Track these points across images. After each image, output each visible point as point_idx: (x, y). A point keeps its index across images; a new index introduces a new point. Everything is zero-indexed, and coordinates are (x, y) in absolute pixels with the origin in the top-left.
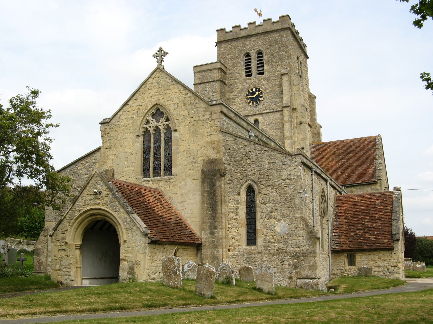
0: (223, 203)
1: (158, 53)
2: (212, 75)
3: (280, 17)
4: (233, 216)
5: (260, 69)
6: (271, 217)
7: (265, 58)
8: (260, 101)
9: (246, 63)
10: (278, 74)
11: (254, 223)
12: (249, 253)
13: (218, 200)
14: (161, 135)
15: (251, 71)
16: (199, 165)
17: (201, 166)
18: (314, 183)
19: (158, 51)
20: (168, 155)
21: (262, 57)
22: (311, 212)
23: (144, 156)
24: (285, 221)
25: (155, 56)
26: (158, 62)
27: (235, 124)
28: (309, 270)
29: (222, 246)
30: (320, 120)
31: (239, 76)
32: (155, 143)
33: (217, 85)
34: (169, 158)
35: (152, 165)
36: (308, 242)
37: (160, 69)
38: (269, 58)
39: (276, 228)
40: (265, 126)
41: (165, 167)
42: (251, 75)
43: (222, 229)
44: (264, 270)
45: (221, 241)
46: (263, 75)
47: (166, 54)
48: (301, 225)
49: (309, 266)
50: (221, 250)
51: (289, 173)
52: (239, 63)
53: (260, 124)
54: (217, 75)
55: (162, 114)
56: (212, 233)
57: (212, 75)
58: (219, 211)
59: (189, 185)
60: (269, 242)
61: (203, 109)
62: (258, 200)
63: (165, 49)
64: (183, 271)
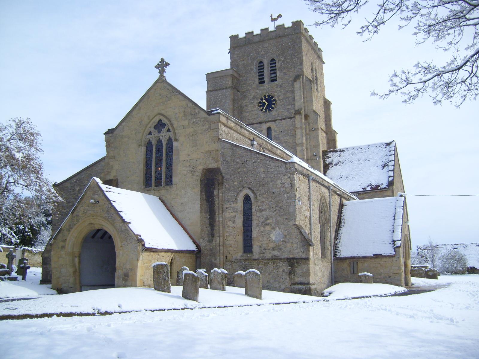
0: (221, 212)
1: (160, 64)
2: (224, 82)
3: (246, 34)
4: (230, 223)
5: (273, 75)
6: (267, 224)
7: (278, 65)
8: (272, 108)
9: (259, 70)
10: (291, 81)
11: (250, 231)
12: (245, 260)
13: (216, 209)
14: (162, 146)
15: (263, 78)
16: (198, 174)
17: (200, 175)
18: (311, 191)
19: (160, 62)
20: (169, 165)
21: (275, 63)
22: (307, 220)
23: (146, 166)
24: (279, 229)
25: (157, 67)
26: (159, 72)
27: (235, 133)
28: (303, 276)
29: (220, 253)
30: (335, 126)
31: (252, 83)
32: (156, 154)
33: (229, 92)
34: (170, 167)
35: (153, 175)
36: (302, 250)
37: (161, 80)
38: (281, 65)
39: (271, 235)
40: (278, 133)
41: (166, 176)
42: (263, 82)
43: (219, 237)
44: (251, 277)
45: (218, 248)
46: (276, 82)
47: (167, 64)
48: (296, 232)
49: (302, 272)
50: (219, 257)
51: (284, 182)
52: (252, 69)
53: (273, 131)
54: (230, 82)
55: (163, 125)
56: (211, 241)
57: (224, 82)
58: (217, 220)
59: (189, 194)
60: (265, 249)
61: (202, 120)
62: (254, 209)
63: (166, 60)
64: (178, 278)
